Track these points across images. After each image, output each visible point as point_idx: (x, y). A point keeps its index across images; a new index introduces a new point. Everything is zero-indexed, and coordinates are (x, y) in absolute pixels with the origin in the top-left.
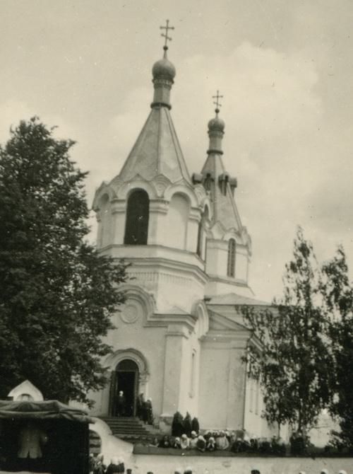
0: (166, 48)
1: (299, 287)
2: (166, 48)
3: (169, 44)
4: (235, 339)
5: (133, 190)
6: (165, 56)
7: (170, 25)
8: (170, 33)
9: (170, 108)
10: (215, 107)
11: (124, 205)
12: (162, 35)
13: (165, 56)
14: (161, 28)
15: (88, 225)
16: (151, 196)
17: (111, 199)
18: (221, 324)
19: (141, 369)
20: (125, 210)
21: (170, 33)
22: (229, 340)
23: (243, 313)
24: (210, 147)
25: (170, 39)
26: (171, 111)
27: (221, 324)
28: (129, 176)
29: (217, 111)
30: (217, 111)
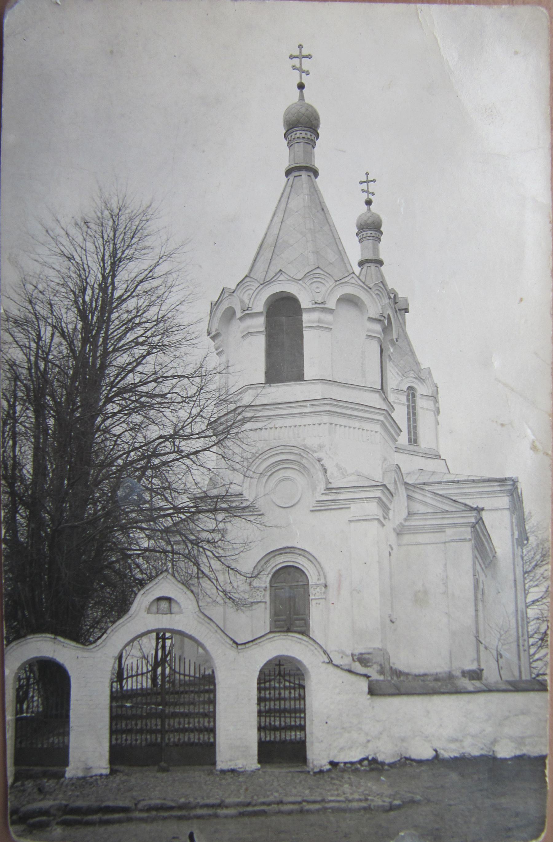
0: (301, 86)
1: (219, 473)
2: (301, 86)
3: (305, 80)
4: (454, 525)
5: (265, 302)
6: (302, 98)
7: (305, 52)
8: (306, 64)
9: (316, 173)
10: (365, 196)
11: (261, 321)
12: (294, 68)
13: (302, 98)
14: (292, 57)
15: (80, 774)
16: (305, 303)
17: (239, 314)
18: (425, 504)
19: (313, 578)
20: (263, 329)
21: (306, 64)
22: (440, 529)
23: (517, 488)
24: (362, 254)
25: (308, 73)
26: (318, 180)
27: (425, 504)
28: (259, 274)
29: (369, 203)
30: (369, 203)
